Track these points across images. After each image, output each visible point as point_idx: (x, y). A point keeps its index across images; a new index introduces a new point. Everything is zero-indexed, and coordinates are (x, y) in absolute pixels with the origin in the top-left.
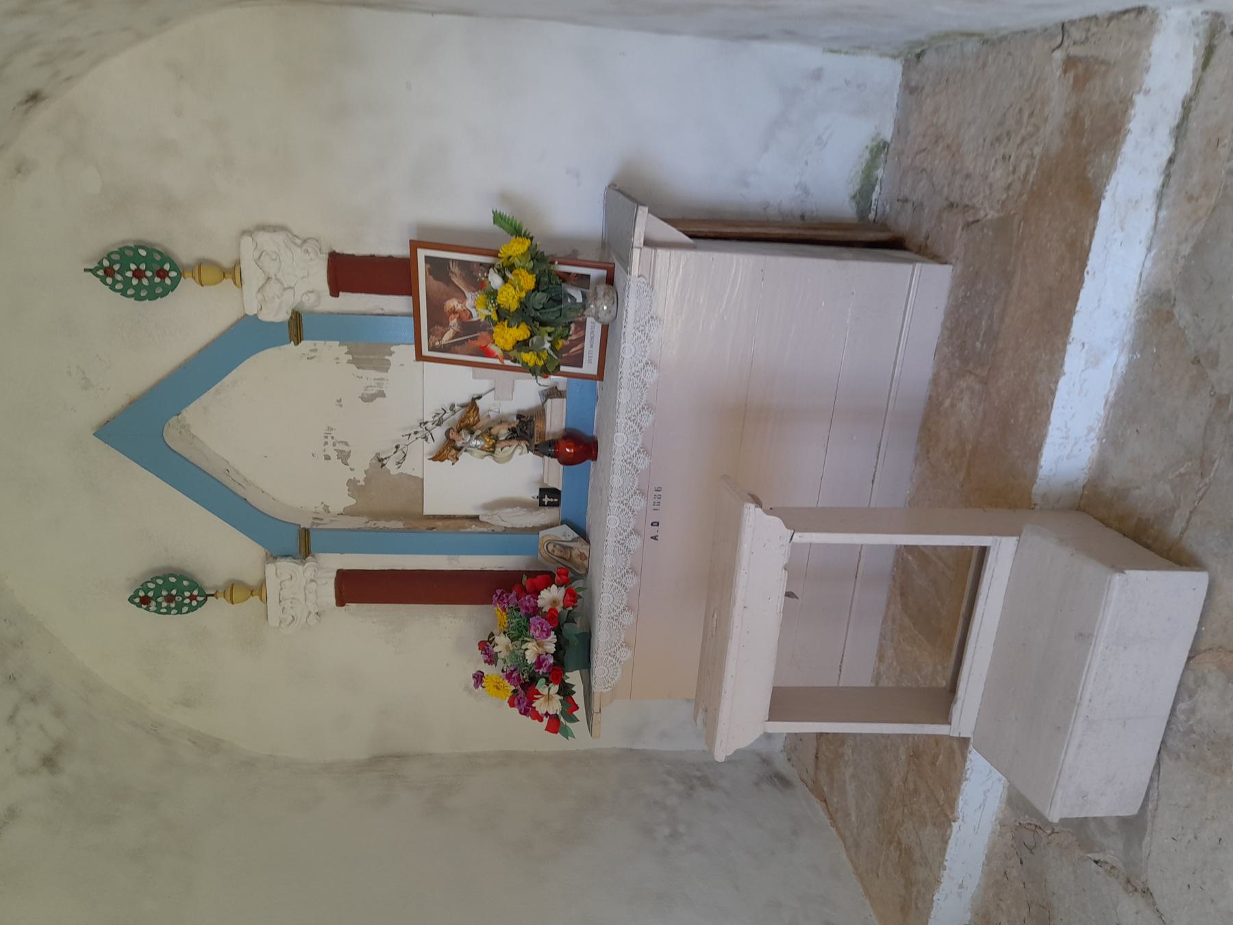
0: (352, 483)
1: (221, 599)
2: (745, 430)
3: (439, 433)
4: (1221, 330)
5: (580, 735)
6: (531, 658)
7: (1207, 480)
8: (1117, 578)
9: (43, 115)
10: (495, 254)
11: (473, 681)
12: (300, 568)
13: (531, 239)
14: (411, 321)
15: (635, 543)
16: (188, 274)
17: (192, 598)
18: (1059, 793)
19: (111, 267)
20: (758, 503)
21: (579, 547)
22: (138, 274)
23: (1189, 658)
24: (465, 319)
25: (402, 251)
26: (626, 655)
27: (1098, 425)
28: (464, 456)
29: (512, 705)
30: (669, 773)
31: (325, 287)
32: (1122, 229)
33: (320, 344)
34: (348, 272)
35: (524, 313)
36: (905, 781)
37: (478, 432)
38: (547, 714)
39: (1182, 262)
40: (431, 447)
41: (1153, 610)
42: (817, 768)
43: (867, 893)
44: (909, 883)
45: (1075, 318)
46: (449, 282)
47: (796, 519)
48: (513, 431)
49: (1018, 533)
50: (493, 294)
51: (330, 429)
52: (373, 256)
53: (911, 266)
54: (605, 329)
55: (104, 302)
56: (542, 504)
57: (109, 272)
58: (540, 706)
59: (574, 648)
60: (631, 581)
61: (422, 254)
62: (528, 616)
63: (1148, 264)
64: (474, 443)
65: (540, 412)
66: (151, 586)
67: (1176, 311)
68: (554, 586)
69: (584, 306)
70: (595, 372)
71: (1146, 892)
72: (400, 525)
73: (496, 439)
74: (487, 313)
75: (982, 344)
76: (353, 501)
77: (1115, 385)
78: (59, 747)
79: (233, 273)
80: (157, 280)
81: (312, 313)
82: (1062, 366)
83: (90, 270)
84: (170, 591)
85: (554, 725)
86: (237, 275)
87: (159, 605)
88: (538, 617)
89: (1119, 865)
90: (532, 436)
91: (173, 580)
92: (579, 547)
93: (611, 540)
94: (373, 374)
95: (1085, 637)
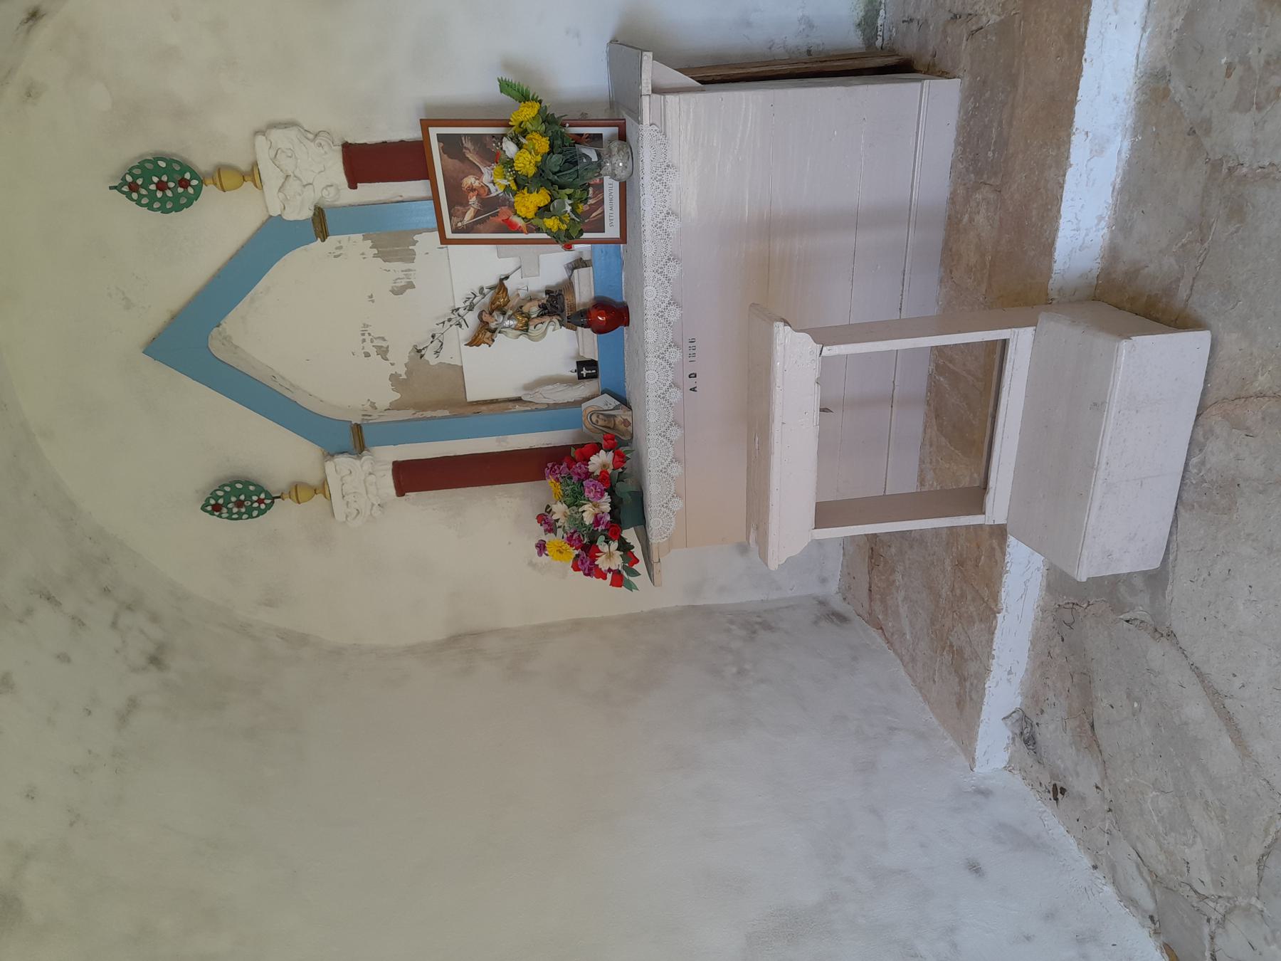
0: (394, 378)
1: (288, 500)
2: (769, 271)
3: (472, 318)
4: (1212, 97)
5: (644, 596)
6: (588, 519)
7: (1206, 245)
8: (1125, 345)
9: (45, 32)
10: (506, 124)
11: (536, 551)
12: (358, 463)
13: (540, 102)
14: (431, 204)
15: (675, 396)
16: (208, 181)
17: (260, 501)
18: (1085, 552)
19: (134, 182)
20: (786, 323)
21: (622, 414)
22: (161, 186)
23: (1198, 416)
24: (484, 196)
25: (414, 134)
26: (677, 505)
27: (1107, 213)
28: (499, 338)
29: (576, 568)
30: (732, 622)
31: (342, 179)
32: (1116, 11)
33: (344, 238)
34: (364, 162)
35: (542, 178)
36: (953, 590)
37: (510, 313)
38: (610, 570)
39: (1175, 36)
40: (465, 333)
41: (1158, 374)
42: (871, 599)
43: (926, 699)
44: (962, 679)
45: (1077, 108)
46: (463, 159)
47: (823, 336)
48: (543, 307)
49: (1033, 323)
50: (510, 163)
51: (366, 326)
52: (385, 142)
53: (919, 84)
54: (623, 187)
55: (131, 218)
56: (581, 377)
57: (133, 187)
58: (602, 563)
59: (628, 508)
60: (675, 434)
61: (434, 132)
62: (581, 481)
63: (1144, 45)
64: (507, 323)
65: (568, 285)
66: (220, 493)
67: (1171, 86)
68: (602, 452)
69: (600, 165)
70: (618, 236)
71: (1171, 635)
72: (446, 413)
73: (528, 317)
74: (505, 182)
75: (994, 152)
76: (399, 396)
77: (1120, 171)
78: (161, 647)
79: (251, 175)
80: (180, 190)
81: (334, 208)
82: (1068, 158)
83: (115, 188)
84: (238, 498)
85: (618, 580)
86: (257, 176)
87: (230, 511)
88: (590, 485)
89: (1148, 618)
90: (563, 311)
91: (239, 486)
92: (622, 414)
93: (651, 395)
94: (397, 267)
95: (1099, 406)
